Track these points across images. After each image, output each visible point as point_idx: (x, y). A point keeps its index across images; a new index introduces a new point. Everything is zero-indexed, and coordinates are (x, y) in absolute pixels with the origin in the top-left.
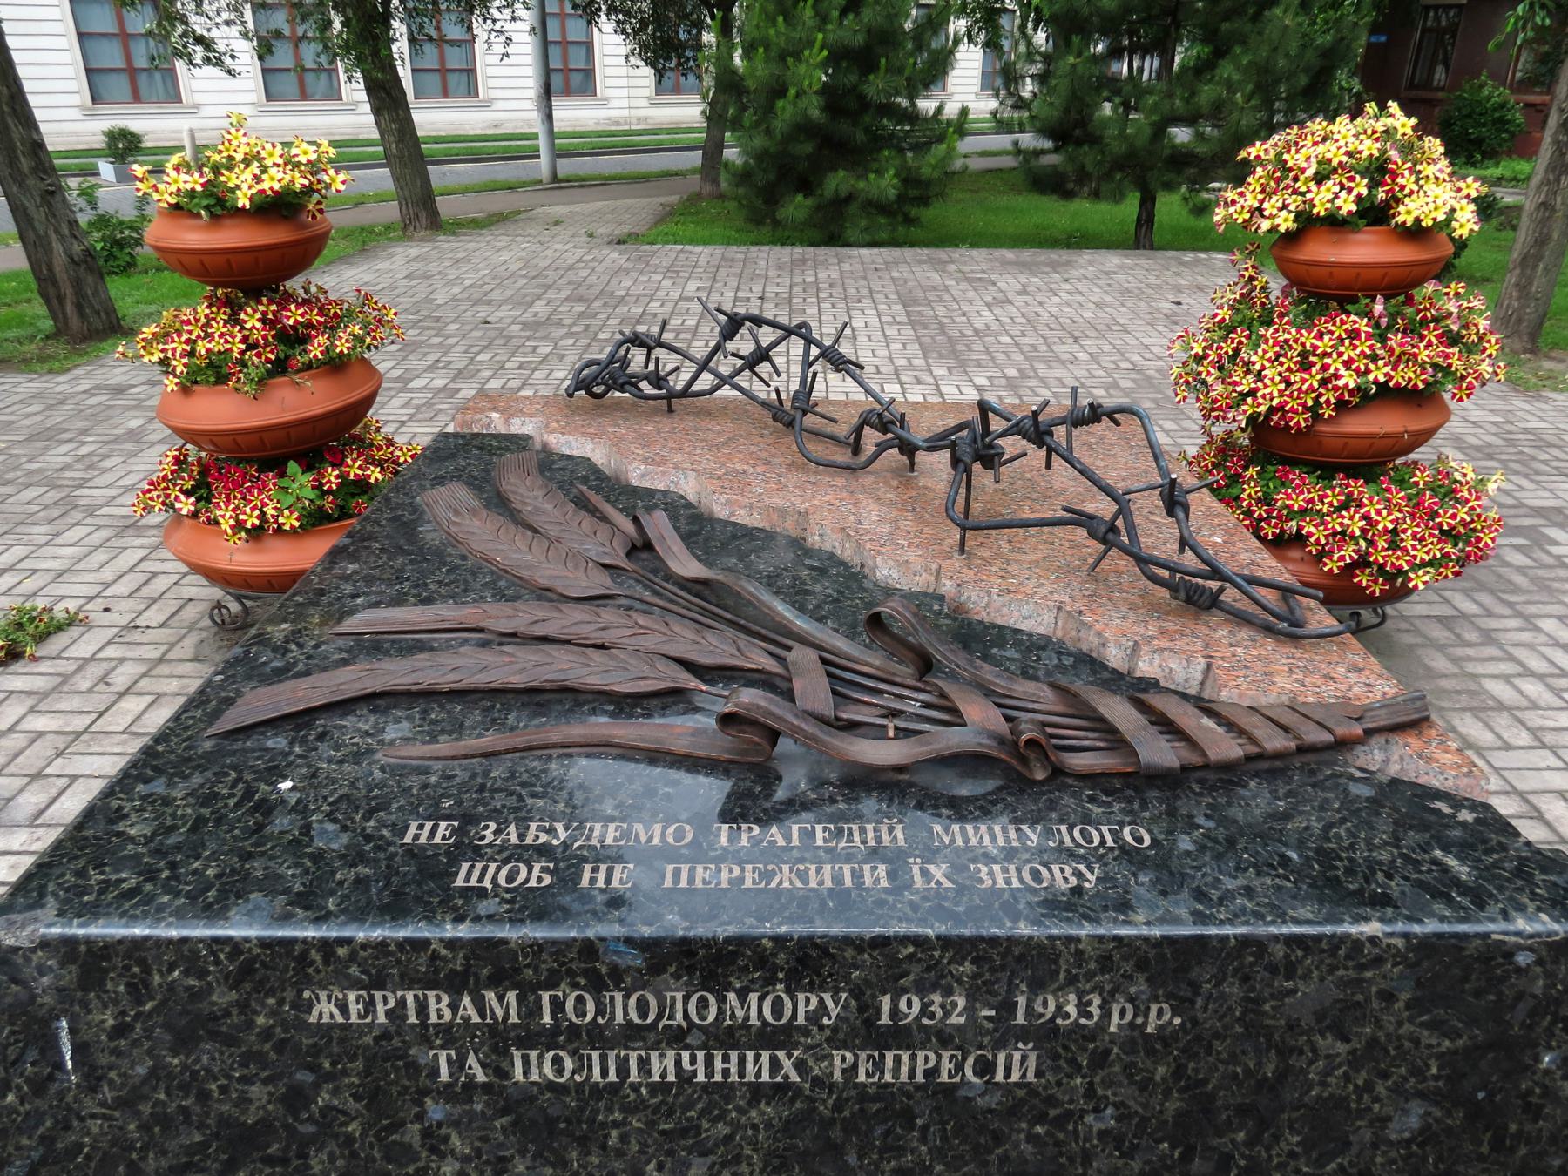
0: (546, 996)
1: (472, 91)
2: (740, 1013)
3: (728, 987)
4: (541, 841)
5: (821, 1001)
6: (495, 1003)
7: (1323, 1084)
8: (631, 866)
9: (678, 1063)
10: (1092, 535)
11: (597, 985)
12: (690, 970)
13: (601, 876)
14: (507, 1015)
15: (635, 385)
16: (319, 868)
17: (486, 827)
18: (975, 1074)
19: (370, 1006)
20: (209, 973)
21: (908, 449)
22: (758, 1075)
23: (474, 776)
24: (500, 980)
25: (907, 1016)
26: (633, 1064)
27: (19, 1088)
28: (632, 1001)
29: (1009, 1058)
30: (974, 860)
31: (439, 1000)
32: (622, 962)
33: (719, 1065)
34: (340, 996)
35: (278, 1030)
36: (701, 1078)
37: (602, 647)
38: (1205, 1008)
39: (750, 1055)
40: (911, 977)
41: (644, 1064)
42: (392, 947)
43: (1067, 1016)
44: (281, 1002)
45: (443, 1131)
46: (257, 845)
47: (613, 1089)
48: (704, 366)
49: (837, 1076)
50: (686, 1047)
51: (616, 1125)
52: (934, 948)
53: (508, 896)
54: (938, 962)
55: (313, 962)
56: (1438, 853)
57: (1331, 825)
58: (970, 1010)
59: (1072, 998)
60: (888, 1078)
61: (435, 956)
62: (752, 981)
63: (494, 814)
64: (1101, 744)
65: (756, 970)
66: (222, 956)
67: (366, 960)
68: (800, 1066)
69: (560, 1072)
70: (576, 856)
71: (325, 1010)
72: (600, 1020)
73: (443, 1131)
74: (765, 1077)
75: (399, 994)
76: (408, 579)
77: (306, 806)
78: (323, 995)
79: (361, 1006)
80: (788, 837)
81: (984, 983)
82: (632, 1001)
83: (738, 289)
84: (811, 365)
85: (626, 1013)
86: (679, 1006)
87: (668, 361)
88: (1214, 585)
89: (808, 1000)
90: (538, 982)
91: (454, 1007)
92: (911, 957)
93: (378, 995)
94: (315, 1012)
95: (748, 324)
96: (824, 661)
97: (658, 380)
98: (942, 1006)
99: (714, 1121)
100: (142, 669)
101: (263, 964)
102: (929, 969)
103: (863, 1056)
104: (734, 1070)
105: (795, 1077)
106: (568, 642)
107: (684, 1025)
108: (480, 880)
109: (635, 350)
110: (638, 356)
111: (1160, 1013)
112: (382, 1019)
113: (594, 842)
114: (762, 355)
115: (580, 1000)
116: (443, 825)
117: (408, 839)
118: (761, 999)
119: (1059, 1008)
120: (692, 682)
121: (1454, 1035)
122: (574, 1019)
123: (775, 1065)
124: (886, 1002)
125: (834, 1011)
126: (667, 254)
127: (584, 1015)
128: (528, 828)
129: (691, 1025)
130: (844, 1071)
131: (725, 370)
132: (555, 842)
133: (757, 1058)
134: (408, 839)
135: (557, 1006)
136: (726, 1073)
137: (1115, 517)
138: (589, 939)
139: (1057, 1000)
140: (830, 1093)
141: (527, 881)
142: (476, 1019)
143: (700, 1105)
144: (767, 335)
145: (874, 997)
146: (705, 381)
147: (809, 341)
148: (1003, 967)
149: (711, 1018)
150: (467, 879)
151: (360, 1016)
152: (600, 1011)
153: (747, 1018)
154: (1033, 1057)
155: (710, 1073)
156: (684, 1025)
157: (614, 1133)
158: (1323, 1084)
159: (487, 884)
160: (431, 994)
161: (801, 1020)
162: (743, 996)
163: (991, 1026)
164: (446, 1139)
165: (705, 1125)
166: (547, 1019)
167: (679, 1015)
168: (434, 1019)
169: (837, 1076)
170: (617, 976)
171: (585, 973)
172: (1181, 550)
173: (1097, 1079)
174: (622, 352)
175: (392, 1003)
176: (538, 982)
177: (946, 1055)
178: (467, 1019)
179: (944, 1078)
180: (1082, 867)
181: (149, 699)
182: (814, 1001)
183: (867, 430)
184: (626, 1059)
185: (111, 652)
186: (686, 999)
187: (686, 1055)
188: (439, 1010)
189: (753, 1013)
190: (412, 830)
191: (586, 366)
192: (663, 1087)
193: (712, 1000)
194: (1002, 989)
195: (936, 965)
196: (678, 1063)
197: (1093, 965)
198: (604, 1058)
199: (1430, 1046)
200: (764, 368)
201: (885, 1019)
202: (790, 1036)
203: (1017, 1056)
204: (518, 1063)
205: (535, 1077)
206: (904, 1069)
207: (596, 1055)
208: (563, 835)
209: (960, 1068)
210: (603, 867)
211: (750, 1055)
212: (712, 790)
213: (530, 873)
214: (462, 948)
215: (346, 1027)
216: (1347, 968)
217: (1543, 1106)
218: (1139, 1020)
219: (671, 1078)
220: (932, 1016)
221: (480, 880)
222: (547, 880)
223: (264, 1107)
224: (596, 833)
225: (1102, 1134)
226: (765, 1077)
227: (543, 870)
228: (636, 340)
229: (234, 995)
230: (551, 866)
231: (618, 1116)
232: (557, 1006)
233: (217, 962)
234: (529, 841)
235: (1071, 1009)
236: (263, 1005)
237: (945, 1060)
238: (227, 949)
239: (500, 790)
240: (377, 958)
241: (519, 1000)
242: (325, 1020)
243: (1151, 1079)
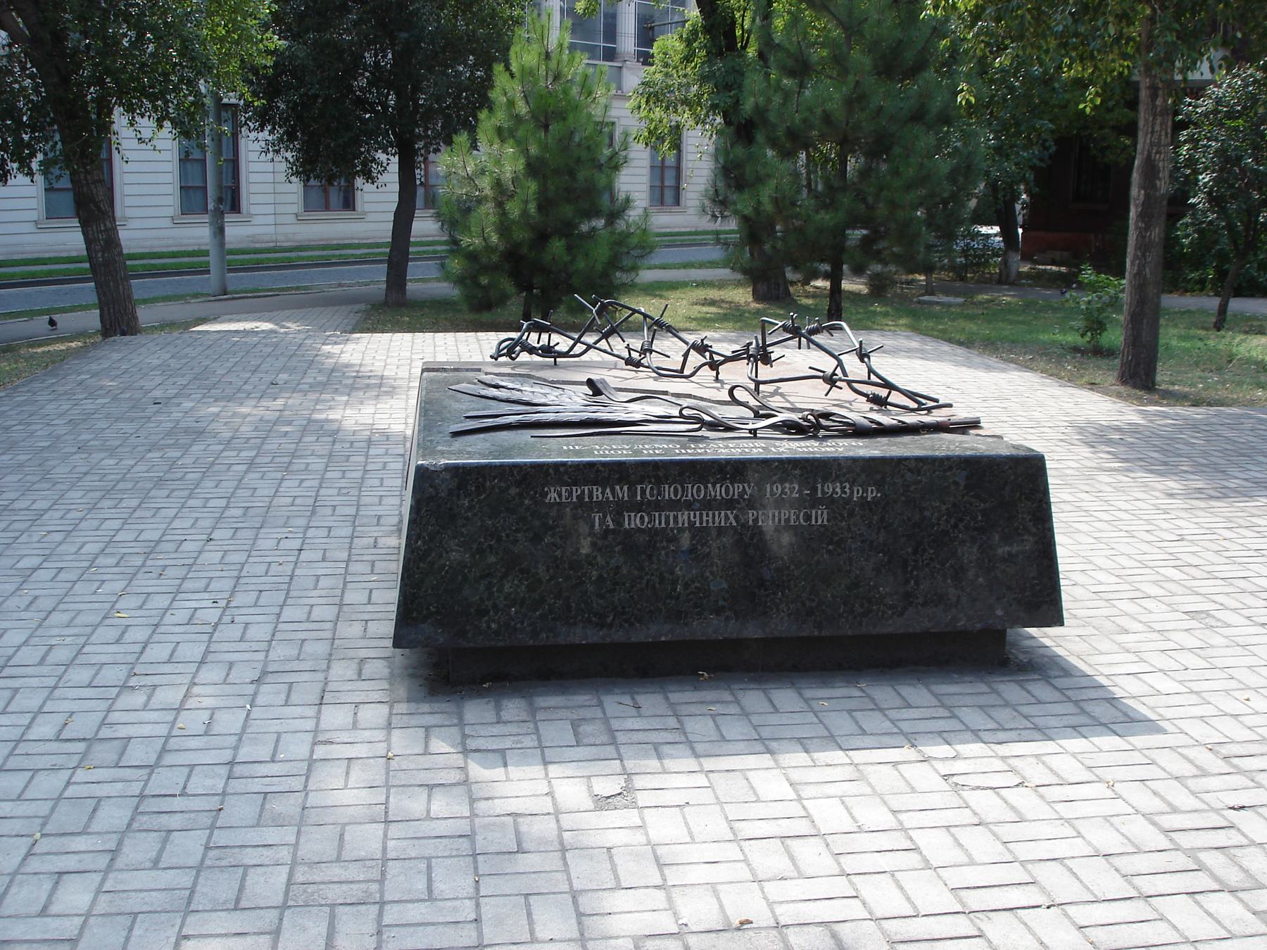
19: (571, 494)
58: (800, 491)
61: (598, 471)
91: (603, 493)
212: (229, 218)
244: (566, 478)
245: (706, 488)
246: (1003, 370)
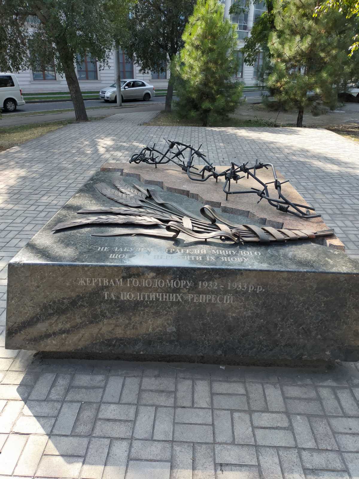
0: (128, 280)
1: (96, 78)
2: (169, 285)
6: (118, 281)
7: (297, 307)
9: (156, 296)
15: (147, 160)
18: (220, 301)
21: (216, 176)
22: (173, 299)
26: (146, 296)
27: (15, 299)
29: (227, 297)
30: (221, 256)
31: (106, 281)
33: (164, 297)
36: (160, 300)
38: (270, 288)
39: (171, 295)
41: (149, 296)
43: (239, 288)
45: (105, 311)
47: (142, 301)
49: (190, 300)
50: (158, 292)
51: (142, 310)
56: (327, 259)
57: (303, 253)
58: (218, 286)
60: (201, 301)
68: (182, 297)
69: (131, 298)
73: (105, 311)
74: (174, 300)
82: (147, 281)
83: (175, 138)
85: (145, 284)
86: (156, 283)
87: (156, 154)
88: (286, 206)
91: (109, 282)
94: (80, 283)
95: (176, 144)
97: (153, 159)
99: (163, 310)
100: (17, 233)
103: (195, 295)
104: (168, 298)
105: (181, 300)
109: (147, 152)
110: (148, 152)
111: (260, 288)
112: (94, 284)
114: (180, 153)
115: (136, 281)
116: (106, 248)
117: (99, 250)
118: (174, 281)
119: (238, 286)
120: (160, 222)
121: (327, 297)
123: (176, 297)
126: (154, 129)
130: (191, 299)
133: (173, 295)
134: (99, 250)
135: (131, 282)
136: (166, 299)
137: (264, 190)
140: (188, 304)
143: (160, 306)
146: (165, 160)
147: (192, 149)
152: (140, 284)
153: (171, 286)
154: (232, 297)
155: (162, 299)
157: (142, 312)
158: (297, 307)
160: (104, 279)
161: (182, 287)
164: (105, 313)
165: (161, 311)
167: (156, 285)
168: (105, 285)
169: (190, 300)
172: (279, 198)
173: (246, 303)
174: (144, 152)
177: (213, 296)
179: (213, 301)
181: (20, 240)
182: (185, 282)
184: (145, 295)
185: (8, 228)
187: (157, 294)
189: (172, 285)
190: (100, 248)
191: (135, 155)
192: (152, 302)
193: (163, 281)
196: (156, 296)
198: (140, 294)
199: (322, 299)
200: (181, 157)
202: (180, 290)
203: (229, 297)
204: (122, 295)
205: (125, 299)
206: (204, 299)
207: (138, 294)
209: (216, 299)
211: (171, 295)
215: (86, 286)
216: (301, 279)
217: (349, 315)
218: (255, 290)
219: (154, 300)
223: (67, 305)
225: (248, 317)
226: (174, 300)
231: (142, 308)
233: (60, 271)
235: (240, 286)
237: (213, 297)
243: (258, 304)
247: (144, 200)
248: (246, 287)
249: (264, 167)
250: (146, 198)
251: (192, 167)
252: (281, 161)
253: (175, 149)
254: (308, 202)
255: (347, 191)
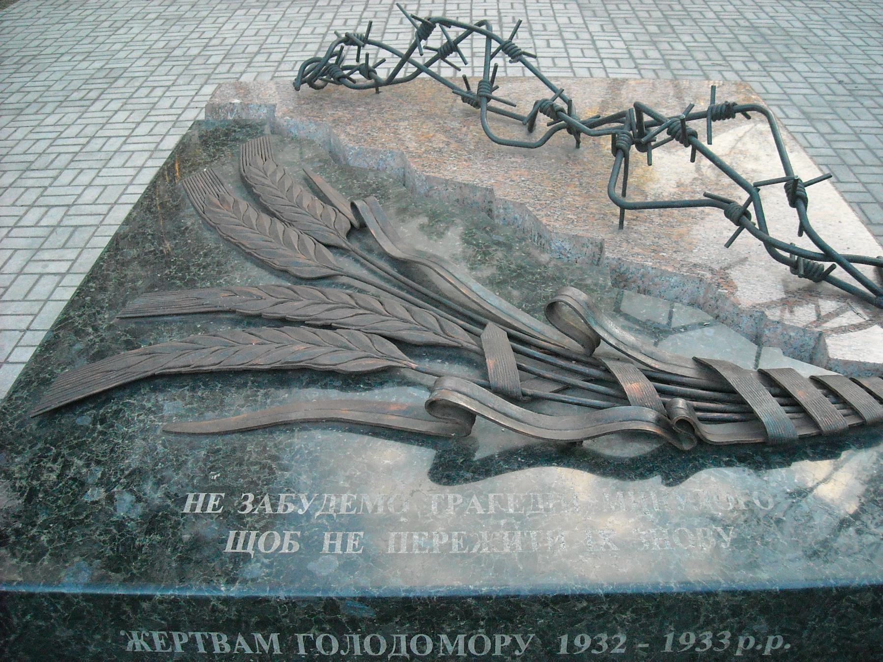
2: (450, 649)
3: (442, 631)
4: (290, 510)
5: (514, 640)
8: (361, 533)
10: (728, 215)
11: (339, 629)
12: (410, 620)
13: (338, 543)
14: (272, 649)
16: (122, 535)
17: (246, 498)
19: (170, 641)
20: (51, 617)
23: (234, 450)
24: (264, 626)
25: (580, 649)
28: (367, 639)
31: (220, 639)
32: (357, 615)
34: (147, 634)
35: (105, 655)
37: (329, 327)
38: (809, 638)
40: (584, 623)
42: (182, 603)
44: (105, 637)
46: (76, 514)
48: (406, 59)
52: (602, 603)
53: (266, 561)
54: (606, 613)
55: (125, 612)
58: (629, 645)
59: (709, 634)
61: (214, 610)
62: (460, 627)
63: (253, 486)
64: (736, 417)
65: (462, 620)
66: (59, 607)
67: (163, 611)
70: (317, 525)
71: (136, 643)
72: (342, 653)
75: (191, 633)
76: (174, 263)
77: (109, 479)
78: (135, 634)
79: (163, 641)
80: (485, 505)
81: (641, 626)
84: (492, 56)
85: (362, 648)
89: (503, 640)
90: (294, 627)
91: (232, 643)
92: (584, 609)
93: (175, 635)
94: (130, 644)
96: (511, 337)
98: (608, 642)
101: (89, 612)
102: (598, 617)
106: (302, 323)
107: (408, 656)
108: (245, 546)
110: (350, 56)
112: (179, 649)
113: (331, 511)
114: (451, 47)
115: (326, 640)
116: (213, 496)
118: (467, 639)
122: (323, 652)
124: (564, 639)
125: (523, 647)
127: (331, 649)
128: (278, 499)
129: (413, 656)
131: (420, 61)
132: (300, 512)
135: (310, 644)
137: (747, 204)
138: (331, 599)
139: (697, 635)
141: (280, 548)
142: (249, 651)
144: (454, 33)
145: (554, 636)
147: (490, 37)
148: (656, 615)
149: (428, 652)
150: (234, 547)
151: (163, 648)
152: (342, 646)
156: (408, 656)
159: (250, 549)
160: (214, 635)
162: (452, 637)
163: (645, 654)
166: (302, 651)
168: (217, 650)
170: (354, 623)
171: (329, 621)
172: (800, 234)
175: (185, 640)
176: (294, 627)
178: (242, 651)
180: (719, 529)
182: (508, 640)
183: (541, 116)
186: (408, 639)
188: (220, 645)
190: (190, 501)
193: (428, 639)
194: (654, 629)
195: (604, 614)
197: (726, 611)
200: (452, 58)
201: (563, 650)
208: (306, 505)
210: (340, 535)
212: (425, 456)
213: (282, 541)
214: (235, 604)
215: (153, 655)
218: (759, 647)
220: (600, 648)
221: (245, 546)
222: (296, 547)
224: (332, 504)
227: (293, 537)
228: (349, 40)
229: (71, 632)
230: (299, 533)
232: (310, 644)
233: (56, 610)
234: (280, 510)
235: (708, 642)
236: (93, 639)
238: (62, 602)
239: (256, 464)
240: (171, 610)
241: (280, 639)
242: (138, 649)
244: (155, 617)
245: (436, 640)
246: (711, 361)
247: (343, 242)
248: (726, 641)
249: (739, 115)
250: (349, 234)
251: (548, 263)
252: (727, 27)
253: (436, 39)
254: (820, 160)
255: (801, 21)
